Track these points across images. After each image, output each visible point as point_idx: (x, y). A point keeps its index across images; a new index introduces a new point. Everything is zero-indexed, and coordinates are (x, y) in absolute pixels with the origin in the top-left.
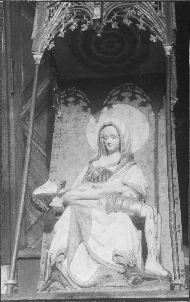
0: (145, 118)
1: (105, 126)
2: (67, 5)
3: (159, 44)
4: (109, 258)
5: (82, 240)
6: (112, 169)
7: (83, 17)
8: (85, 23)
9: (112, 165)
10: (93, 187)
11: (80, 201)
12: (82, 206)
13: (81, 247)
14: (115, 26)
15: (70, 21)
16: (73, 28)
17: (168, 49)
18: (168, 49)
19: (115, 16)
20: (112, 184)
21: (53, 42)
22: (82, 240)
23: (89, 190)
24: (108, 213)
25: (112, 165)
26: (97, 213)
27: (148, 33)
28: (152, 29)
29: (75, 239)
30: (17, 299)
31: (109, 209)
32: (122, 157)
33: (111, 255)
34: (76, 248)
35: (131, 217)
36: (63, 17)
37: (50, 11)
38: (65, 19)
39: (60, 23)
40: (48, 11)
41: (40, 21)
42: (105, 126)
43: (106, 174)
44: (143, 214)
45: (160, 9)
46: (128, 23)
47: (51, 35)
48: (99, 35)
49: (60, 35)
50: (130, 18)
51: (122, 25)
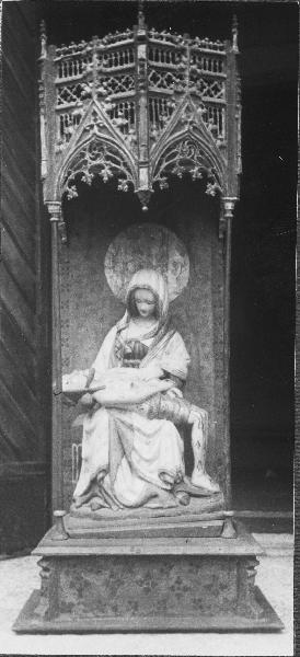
3: (217, 200)
4: (155, 477)
6: (148, 343)
8: (124, 177)
9: (145, 337)
16: (106, 173)
25: (145, 337)
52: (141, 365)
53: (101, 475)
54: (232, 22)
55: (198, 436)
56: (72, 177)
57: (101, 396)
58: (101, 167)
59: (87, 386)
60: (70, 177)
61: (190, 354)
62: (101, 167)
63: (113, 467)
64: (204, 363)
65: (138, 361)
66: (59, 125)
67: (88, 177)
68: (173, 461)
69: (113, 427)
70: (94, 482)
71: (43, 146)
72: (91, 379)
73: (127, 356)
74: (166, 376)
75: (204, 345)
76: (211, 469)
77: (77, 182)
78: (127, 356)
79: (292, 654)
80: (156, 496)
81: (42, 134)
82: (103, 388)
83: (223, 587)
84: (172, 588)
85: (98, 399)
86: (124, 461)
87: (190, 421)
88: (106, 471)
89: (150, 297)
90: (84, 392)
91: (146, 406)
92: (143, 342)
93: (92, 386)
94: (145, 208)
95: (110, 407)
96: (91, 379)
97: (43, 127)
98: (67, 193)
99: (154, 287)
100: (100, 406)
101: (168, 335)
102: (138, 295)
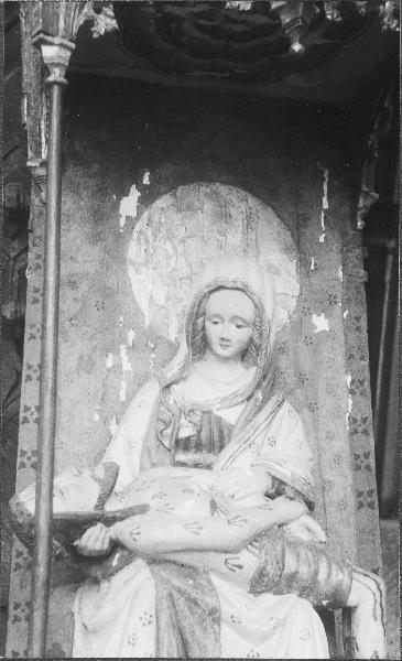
0: (289, 240)
6: (231, 416)
9: (228, 402)
31: (261, 583)
48: (297, 47)
52: (216, 467)
57: (144, 532)
59: (102, 501)
64: (331, 475)
65: (210, 458)
69: (165, 617)
72: (108, 492)
73: (183, 445)
74: (277, 490)
75: (330, 437)
78: (183, 445)
82: (143, 509)
85: (126, 539)
87: (351, 602)
89: (247, 311)
90: (90, 521)
91: (250, 560)
92: (220, 414)
93: (112, 507)
94: (297, 47)
95: (155, 560)
96: (108, 492)
98: (89, 23)
99: (255, 287)
100: (131, 555)
101: (274, 399)
102: (217, 303)
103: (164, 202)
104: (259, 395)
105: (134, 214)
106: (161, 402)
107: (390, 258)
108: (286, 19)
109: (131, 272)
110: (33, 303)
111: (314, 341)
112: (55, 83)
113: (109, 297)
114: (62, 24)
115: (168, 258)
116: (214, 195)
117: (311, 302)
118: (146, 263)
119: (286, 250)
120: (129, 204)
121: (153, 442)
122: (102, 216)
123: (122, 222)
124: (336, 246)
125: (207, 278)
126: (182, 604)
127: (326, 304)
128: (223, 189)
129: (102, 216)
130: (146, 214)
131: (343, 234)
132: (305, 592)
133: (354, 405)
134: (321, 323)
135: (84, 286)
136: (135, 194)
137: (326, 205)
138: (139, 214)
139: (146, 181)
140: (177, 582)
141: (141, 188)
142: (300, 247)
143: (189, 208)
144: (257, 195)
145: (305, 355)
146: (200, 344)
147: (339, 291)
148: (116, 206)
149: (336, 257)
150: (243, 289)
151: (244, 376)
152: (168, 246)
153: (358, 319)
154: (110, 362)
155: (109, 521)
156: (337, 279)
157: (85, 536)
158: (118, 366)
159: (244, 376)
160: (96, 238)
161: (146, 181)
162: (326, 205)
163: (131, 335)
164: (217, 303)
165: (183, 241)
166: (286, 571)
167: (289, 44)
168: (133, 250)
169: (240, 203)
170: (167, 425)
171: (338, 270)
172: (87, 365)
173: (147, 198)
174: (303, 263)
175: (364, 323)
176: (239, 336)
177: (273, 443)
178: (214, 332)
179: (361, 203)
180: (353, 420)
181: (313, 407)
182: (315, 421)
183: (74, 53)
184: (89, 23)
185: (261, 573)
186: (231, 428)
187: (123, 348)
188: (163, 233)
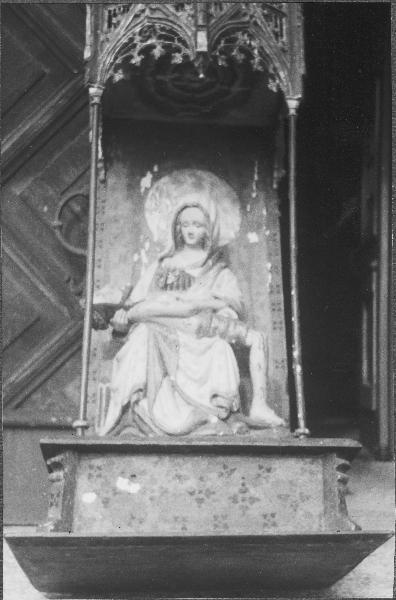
0: (236, 196)
1: (185, 207)
2: (143, 11)
3: (280, 97)
4: (206, 401)
5: (166, 374)
6: (195, 273)
7: (173, 40)
8: (178, 50)
9: (194, 266)
10: (178, 299)
11: (166, 319)
12: (163, 325)
13: (165, 383)
14: (224, 63)
15: (149, 42)
16: (157, 52)
17: (293, 104)
18: (293, 104)
19: (222, 45)
20: (197, 295)
21: (120, 71)
22: (166, 374)
23: (166, 301)
24: (199, 338)
25: (194, 266)
26: (186, 338)
27: (266, 76)
28: (271, 71)
29: (157, 370)
30: (120, 443)
31: (201, 332)
32: (209, 257)
33: (208, 396)
34: (159, 387)
35: (232, 345)
36: (138, 29)
37: (110, 12)
38: (140, 33)
39: (131, 40)
40: (106, 14)
41: (96, 28)
42: (185, 207)
43: (184, 282)
44: (248, 342)
45: (282, 36)
46: (255, 66)
47: (116, 58)
48: (201, 76)
49: (133, 61)
50: (242, 50)
51: (231, 60)
53: (134, 398)
54: (254, 171)
55: (256, 359)
56: (118, 61)
58: (152, 47)
60: (117, 62)
61: (241, 290)
62: (152, 47)
63: (151, 388)
66: (106, 18)
67: (137, 60)
68: (227, 379)
69: (151, 343)
70: (125, 409)
71: (88, 33)
75: (258, 294)
76: (272, 402)
77: (126, 65)
79: (390, 595)
80: (205, 422)
81: (88, 22)
83: (305, 498)
84: (234, 500)
86: (165, 383)
88: (143, 391)
93: (127, 303)
94: (201, 76)
96: (128, 295)
97: (88, 16)
98: (112, 77)
103: (165, 180)
104: (210, 262)
105: (149, 185)
106: (159, 267)
107: (375, 274)
108: (196, 65)
109: (147, 215)
110: (186, 529)
111: (249, 246)
112: (95, 104)
113: (138, 228)
114: (99, 79)
115: (167, 206)
116: (194, 175)
117: (247, 226)
118: (155, 210)
119: (234, 201)
120: (146, 181)
121: (154, 285)
122: (133, 186)
123: (142, 190)
124: (262, 196)
125: (181, 204)
126: (160, 338)
127: (257, 228)
128: (199, 173)
129: (133, 186)
130: (155, 186)
131: (268, 192)
132: (223, 336)
133: (272, 279)
134: (253, 237)
135: (122, 222)
136: (149, 176)
137: (256, 177)
138: (152, 185)
139: (156, 169)
140: (158, 329)
141: (152, 172)
142: (242, 200)
143: (179, 181)
144: (217, 174)
145: (243, 252)
146: (179, 242)
147: (264, 221)
148: (139, 183)
149: (262, 203)
150: (197, 206)
151: (202, 255)
152: (168, 202)
153: (275, 235)
154: (136, 257)
155: (127, 309)
156: (262, 216)
157: (115, 316)
158: (140, 260)
159: (202, 255)
160: (129, 197)
161: (156, 169)
162: (256, 177)
163: (147, 245)
164: (186, 216)
165: (176, 198)
166: (213, 325)
167: (198, 74)
168: (149, 204)
169: (208, 177)
170: (161, 276)
171: (263, 211)
172: (124, 259)
173: (156, 178)
174: (243, 208)
175: (278, 237)
176: (198, 232)
177: (219, 286)
178: (185, 231)
179: (275, 175)
180: (271, 286)
181: (249, 279)
182: (250, 288)
183: (105, 91)
184: (112, 77)
185: (200, 327)
186: (194, 278)
187: (143, 252)
188: (165, 195)
